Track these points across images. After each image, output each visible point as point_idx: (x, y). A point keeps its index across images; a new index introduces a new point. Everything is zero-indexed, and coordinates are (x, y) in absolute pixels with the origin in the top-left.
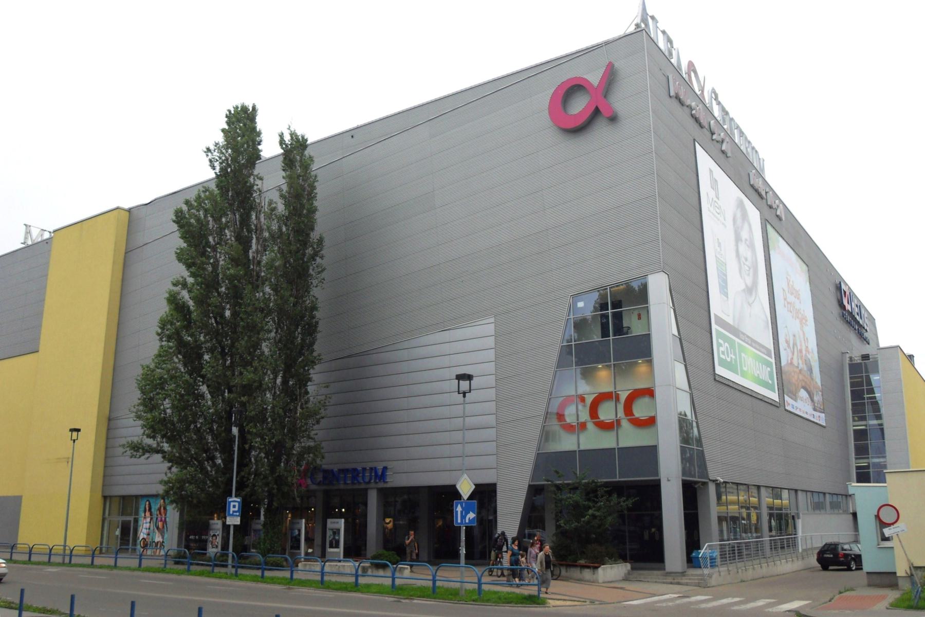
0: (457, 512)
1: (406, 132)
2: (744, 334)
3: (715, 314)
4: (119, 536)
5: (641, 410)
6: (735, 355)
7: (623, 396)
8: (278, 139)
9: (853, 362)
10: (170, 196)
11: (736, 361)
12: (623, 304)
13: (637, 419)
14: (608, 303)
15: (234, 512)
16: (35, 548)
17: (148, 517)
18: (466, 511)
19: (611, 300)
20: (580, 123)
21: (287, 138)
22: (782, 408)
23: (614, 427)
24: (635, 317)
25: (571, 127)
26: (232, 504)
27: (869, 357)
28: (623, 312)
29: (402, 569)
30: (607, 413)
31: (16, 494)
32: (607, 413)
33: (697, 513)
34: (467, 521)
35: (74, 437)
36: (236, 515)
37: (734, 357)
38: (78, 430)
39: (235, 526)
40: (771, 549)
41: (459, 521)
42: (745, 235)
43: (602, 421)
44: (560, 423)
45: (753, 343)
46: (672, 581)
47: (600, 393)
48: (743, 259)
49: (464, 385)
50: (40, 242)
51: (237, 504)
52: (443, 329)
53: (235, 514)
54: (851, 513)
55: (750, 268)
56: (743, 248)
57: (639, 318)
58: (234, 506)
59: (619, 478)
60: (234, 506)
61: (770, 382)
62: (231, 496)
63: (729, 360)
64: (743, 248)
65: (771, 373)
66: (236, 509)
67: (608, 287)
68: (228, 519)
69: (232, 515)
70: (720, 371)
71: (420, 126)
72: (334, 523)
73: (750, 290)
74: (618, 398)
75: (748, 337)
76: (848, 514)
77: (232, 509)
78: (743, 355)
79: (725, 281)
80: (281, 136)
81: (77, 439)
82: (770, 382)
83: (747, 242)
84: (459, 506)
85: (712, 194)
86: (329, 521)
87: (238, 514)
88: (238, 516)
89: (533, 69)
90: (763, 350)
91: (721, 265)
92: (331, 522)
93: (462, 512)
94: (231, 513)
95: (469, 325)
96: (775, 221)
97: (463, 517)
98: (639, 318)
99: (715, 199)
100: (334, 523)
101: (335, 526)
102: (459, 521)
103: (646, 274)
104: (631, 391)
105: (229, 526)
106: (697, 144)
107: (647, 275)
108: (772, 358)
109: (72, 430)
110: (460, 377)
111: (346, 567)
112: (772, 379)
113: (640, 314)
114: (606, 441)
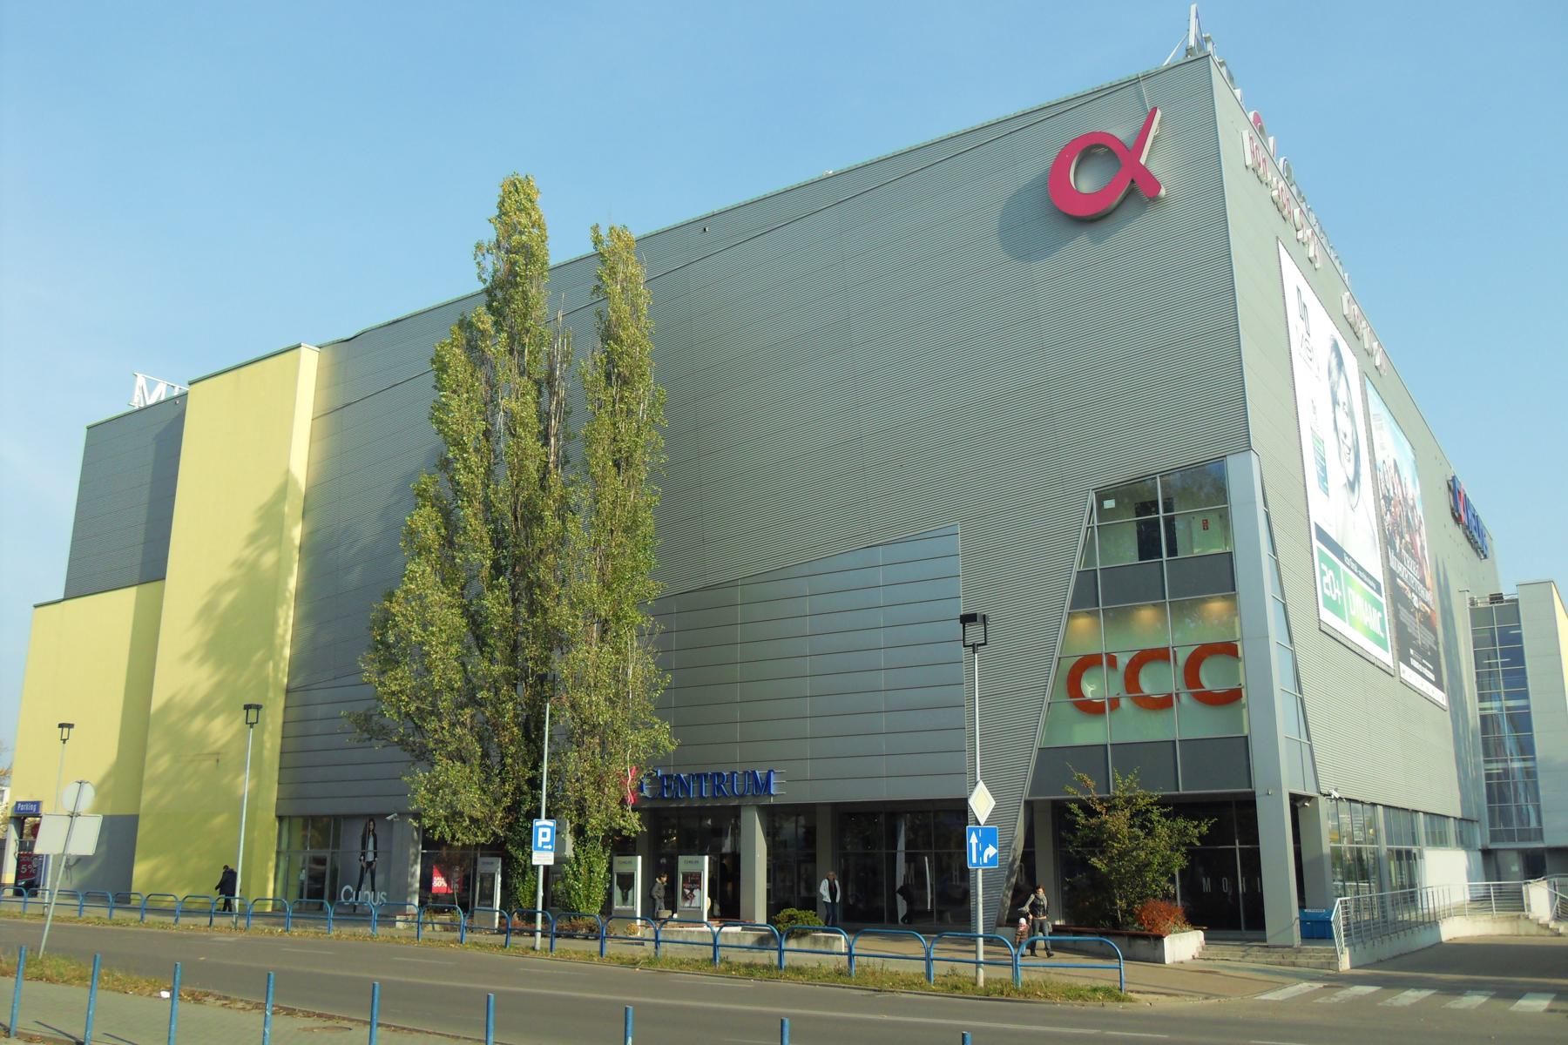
0: (971, 844)
1: (798, 222)
2: (1349, 557)
3: (1316, 524)
4: (306, 883)
5: (1211, 678)
6: (1341, 590)
7: (1123, 661)
8: (590, 234)
9: (1476, 607)
10: (390, 327)
11: (1342, 598)
12: (1176, 507)
13: (1089, 702)
14: (1157, 501)
15: (544, 843)
16: (152, 900)
17: (900, 851)
18: (984, 843)
19: (1162, 496)
20: (1084, 215)
21: (604, 232)
22: (1397, 679)
23: (1172, 705)
24: (1197, 524)
25: (1081, 215)
26: (541, 830)
27: (1502, 598)
28: (1177, 518)
29: (830, 940)
30: (1151, 682)
31: (133, 813)
32: (1151, 682)
33: (1259, 848)
34: (986, 861)
35: (252, 718)
36: (547, 850)
37: (1340, 594)
38: (70, 726)
39: (547, 868)
40: (1393, 905)
41: (974, 861)
42: (1342, 397)
43: (1148, 696)
44: (1073, 700)
45: (1360, 570)
46: (1282, 960)
47: (1203, 645)
48: (1342, 436)
49: (975, 632)
50: (164, 402)
51: (548, 831)
52: (870, 545)
53: (545, 847)
54: (1480, 850)
55: (1350, 450)
56: (1341, 414)
57: (1205, 526)
58: (544, 835)
59: (1183, 790)
60: (544, 835)
61: (1382, 635)
62: (539, 817)
63: (1334, 598)
64: (1341, 414)
65: (1382, 620)
66: (548, 839)
67: (1158, 475)
68: (535, 855)
69: (542, 849)
70: (1327, 616)
71: (819, 214)
72: (488, 863)
73: (1352, 485)
74: (1112, 662)
75: (1354, 562)
76: (1475, 850)
77: (541, 839)
78: (1350, 589)
79: (1324, 469)
80: (596, 228)
81: (257, 722)
82: (1382, 635)
83: (1345, 407)
84: (974, 836)
85: (1301, 324)
86: (682, 859)
87: (550, 847)
88: (552, 850)
89: (1016, 121)
90: (1371, 583)
91: (1318, 441)
92: (484, 863)
93: (977, 845)
94: (540, 845)
95: (916, 538)
96: (1373, 374)
97: (980, 854)
98: (1205, 526)
99: (1306, 336)
100: (488, 863)
101: (625, 869)
102: (974, 861)
103: (1223, 455)
104: (1197, 647)
105: (538, 866)
106: (1280, 243)
107: (1225, 456)
108: (1381, 596)
109: (61, 726)
110: (967, 619)
111: (729, 936)
112: (1384, 630)
113: (1206, 520)
114: (1153, 728)
